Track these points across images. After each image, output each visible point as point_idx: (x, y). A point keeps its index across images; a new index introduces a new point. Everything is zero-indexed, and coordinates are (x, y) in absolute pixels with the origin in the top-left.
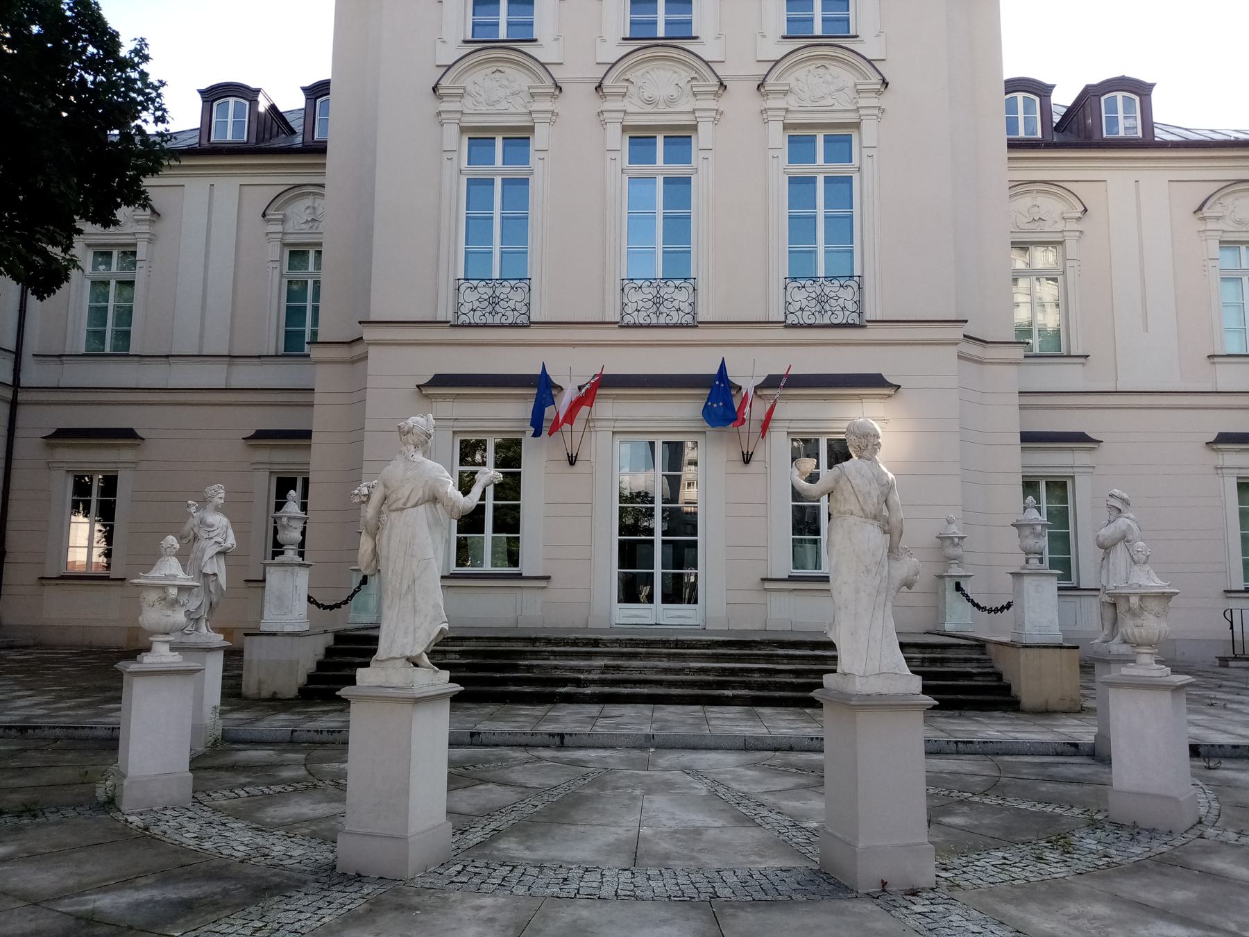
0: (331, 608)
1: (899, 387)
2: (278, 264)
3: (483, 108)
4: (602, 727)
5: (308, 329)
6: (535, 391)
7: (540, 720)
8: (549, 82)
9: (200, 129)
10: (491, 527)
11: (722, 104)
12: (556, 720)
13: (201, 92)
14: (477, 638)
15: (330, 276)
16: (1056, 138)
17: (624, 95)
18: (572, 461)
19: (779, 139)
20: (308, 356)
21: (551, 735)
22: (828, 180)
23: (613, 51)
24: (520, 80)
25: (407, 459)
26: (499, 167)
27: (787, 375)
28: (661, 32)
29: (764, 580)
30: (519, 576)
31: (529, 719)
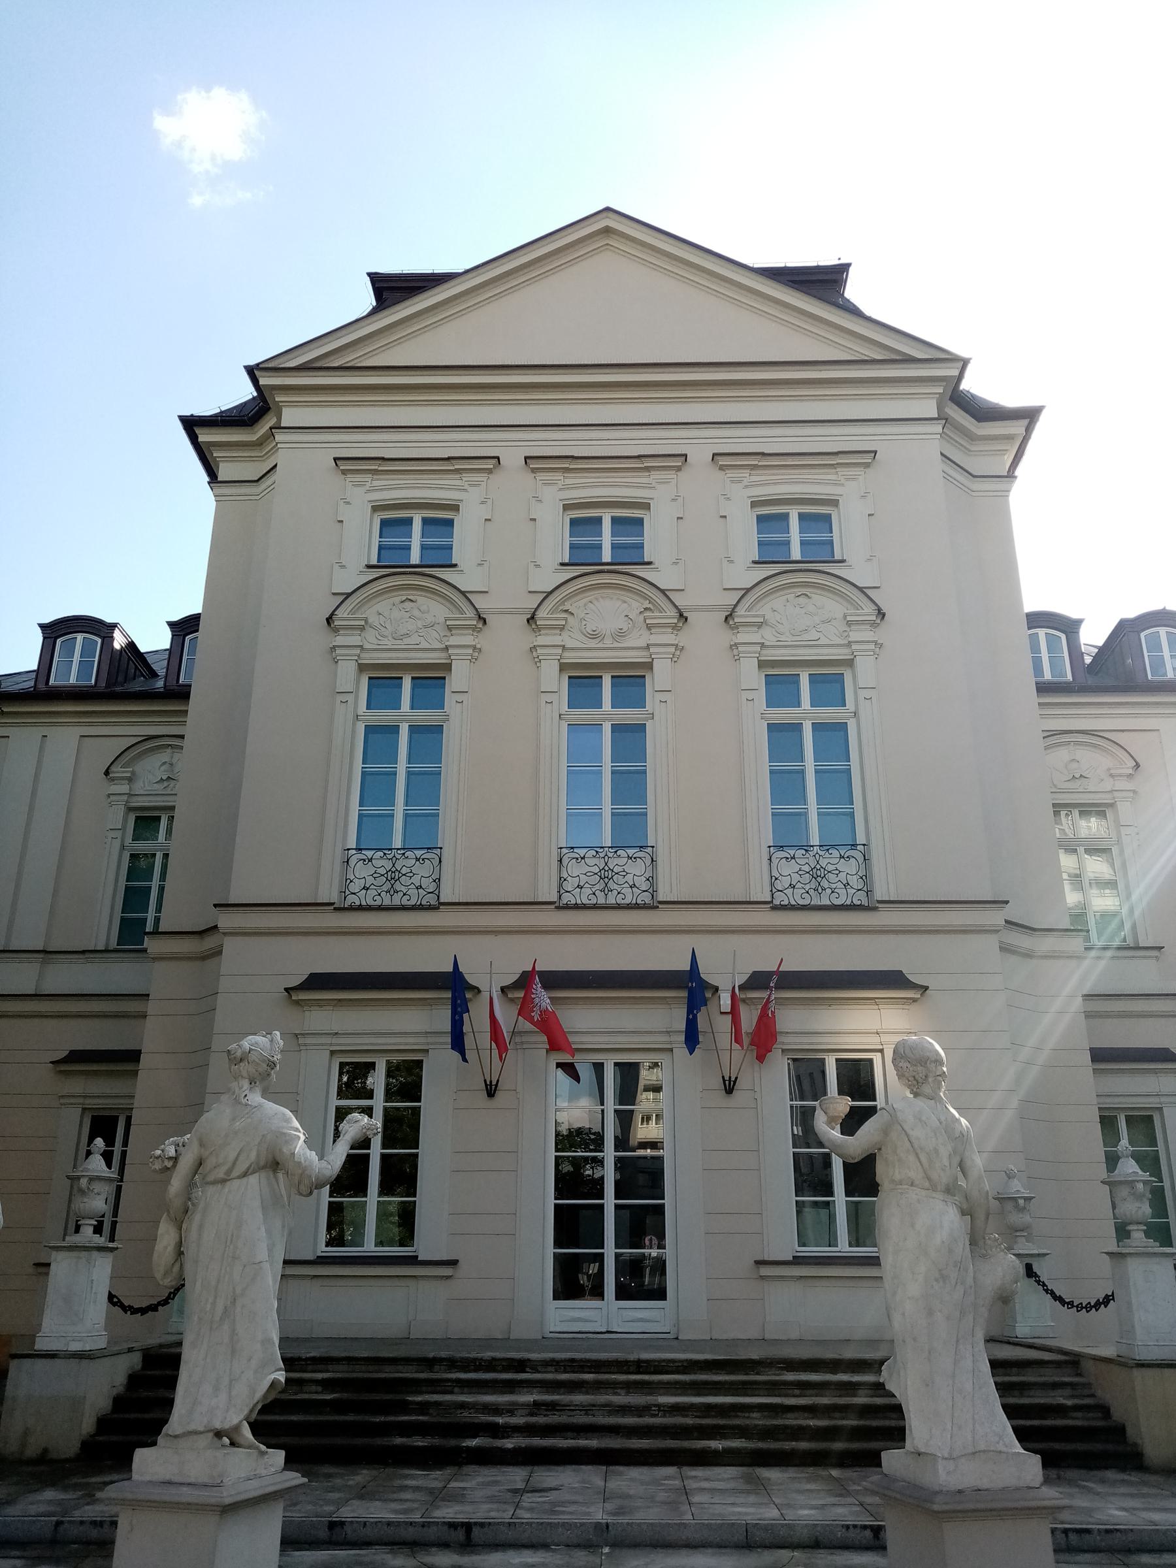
0: (143, 1311)
1: (926, 988)
2: (119, 834)
3: (389, 643)
4: (529, 1511)
5: (151, 915)
6: (449, 995)
7: (437, 1496)
8: (470, 613)
9: (37, 671)
10: (378, 1186)
11: (683, 638)
12: (458, 1497)
13: (42, 627)
14: (349, 1360)
15: (178, 844)
16: (1091, 681)
17: (562, 628)
18: (491, 1091)
19: (754, 679)
20: (145, 950)
21: (453, 1526)
22: (816, 727)
23: (548, 578)
24: (436, 610)
25: (237, 1101)
26: (406, 711)
27: (777, 972)
28: (607, 556)
29: (759, 1263)
30: (413, 1260)
31: (418, 1496)
